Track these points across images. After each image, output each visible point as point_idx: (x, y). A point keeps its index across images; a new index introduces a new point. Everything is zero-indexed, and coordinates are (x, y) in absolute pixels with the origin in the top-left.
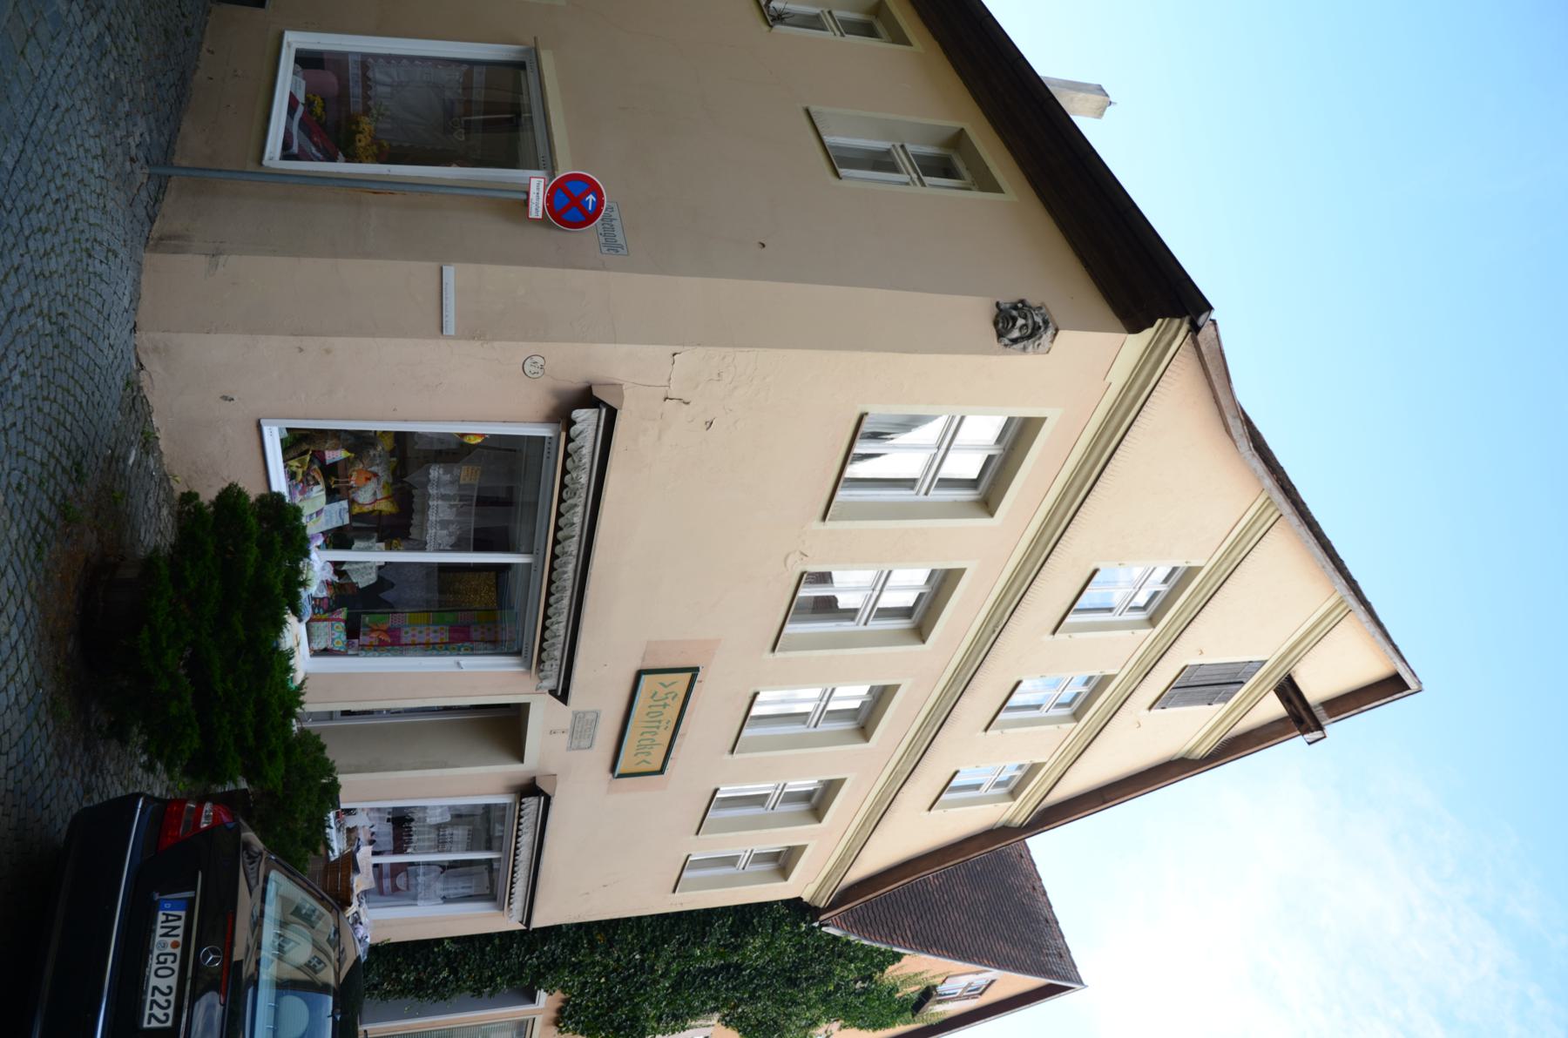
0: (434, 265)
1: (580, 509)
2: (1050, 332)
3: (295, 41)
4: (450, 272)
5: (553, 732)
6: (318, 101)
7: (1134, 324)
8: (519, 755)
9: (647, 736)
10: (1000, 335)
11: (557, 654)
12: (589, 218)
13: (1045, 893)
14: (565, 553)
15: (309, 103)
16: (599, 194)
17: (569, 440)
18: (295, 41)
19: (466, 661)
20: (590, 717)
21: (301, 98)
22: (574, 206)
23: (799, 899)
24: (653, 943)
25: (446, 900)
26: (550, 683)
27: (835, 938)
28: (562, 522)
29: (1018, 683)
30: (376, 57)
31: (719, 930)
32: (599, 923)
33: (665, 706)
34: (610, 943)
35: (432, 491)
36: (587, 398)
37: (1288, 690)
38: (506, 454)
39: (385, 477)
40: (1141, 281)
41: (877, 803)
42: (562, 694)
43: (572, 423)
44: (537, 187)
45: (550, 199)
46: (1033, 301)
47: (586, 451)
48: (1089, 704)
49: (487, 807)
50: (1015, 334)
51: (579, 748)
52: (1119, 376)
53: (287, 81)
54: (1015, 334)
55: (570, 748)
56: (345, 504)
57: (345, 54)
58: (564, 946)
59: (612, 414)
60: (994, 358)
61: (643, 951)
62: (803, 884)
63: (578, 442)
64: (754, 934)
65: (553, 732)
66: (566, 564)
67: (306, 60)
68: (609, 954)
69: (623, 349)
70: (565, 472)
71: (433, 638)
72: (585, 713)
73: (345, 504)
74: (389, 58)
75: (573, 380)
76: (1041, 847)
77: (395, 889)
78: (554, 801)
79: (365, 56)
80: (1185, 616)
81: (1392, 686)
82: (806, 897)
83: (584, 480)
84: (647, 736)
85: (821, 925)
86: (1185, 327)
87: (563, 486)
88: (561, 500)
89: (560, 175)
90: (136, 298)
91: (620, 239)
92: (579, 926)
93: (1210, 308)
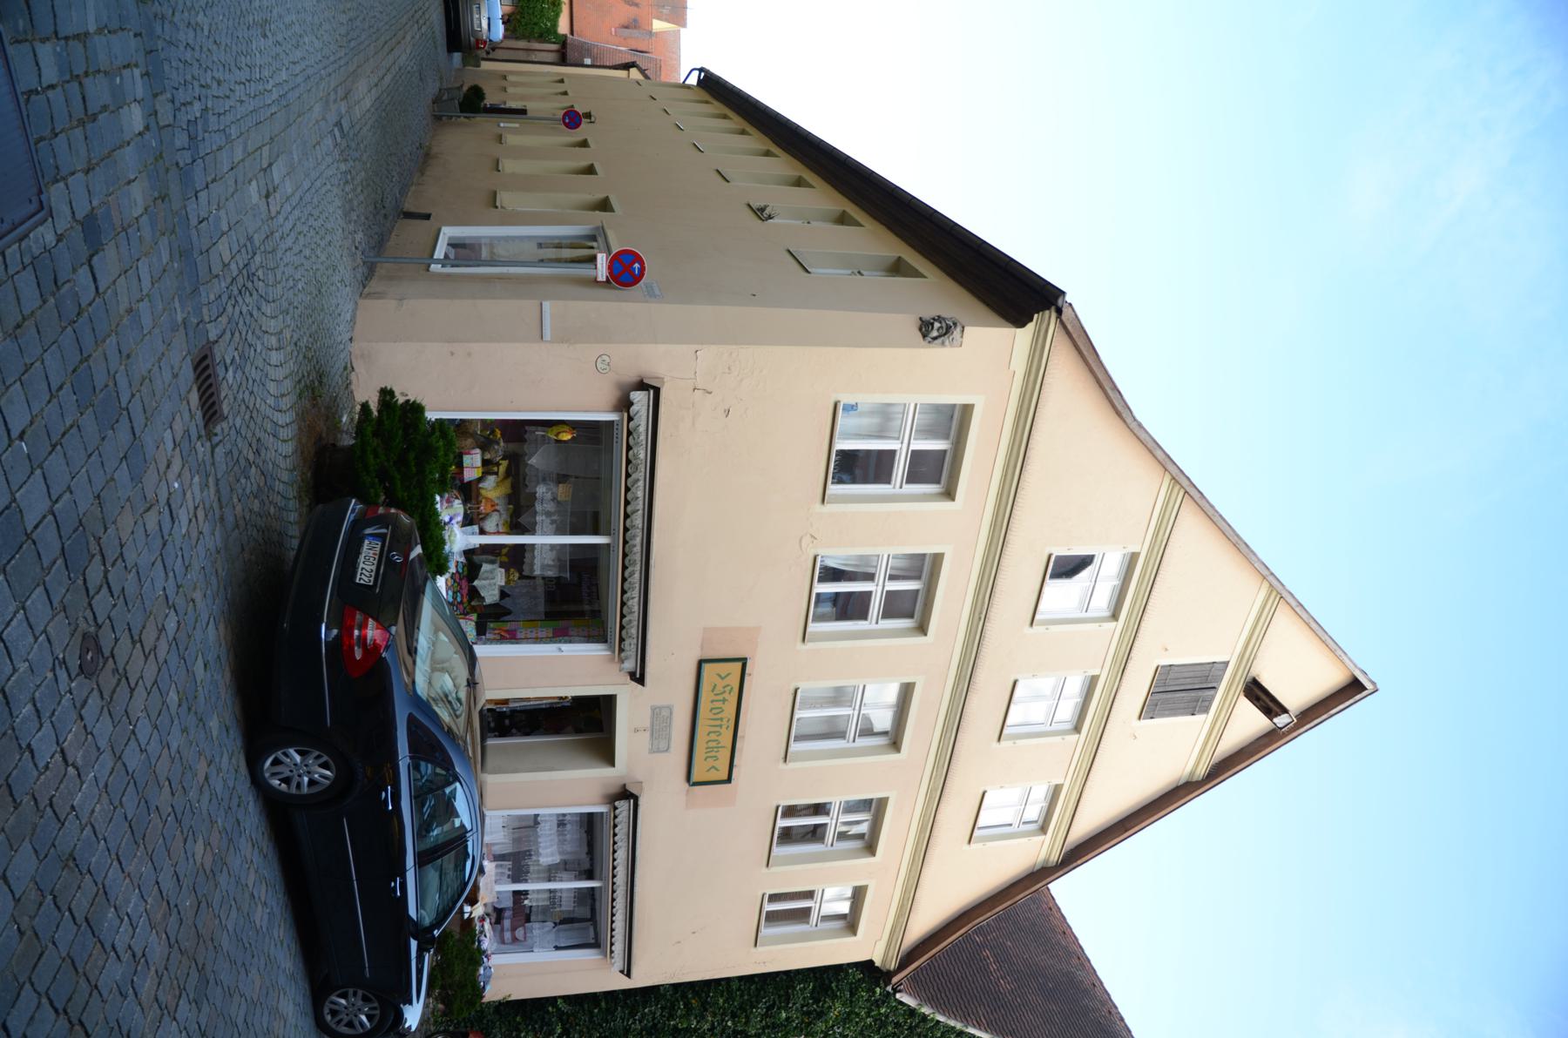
0: (537, 303)
1: (641, 483)
2: (959, 329)
3: (448, 232)
4: (547, 305)
5: (636, 731)
7: (1019, 320)
8: (610, 759)
9: (713, 736)
10: (924, 336)
11: (634, 631)
12: (636, 279)
13: (1122, 1019)
16: (642, 263)
17: (630, 419)
19: (565, 647)
20: (665, 713)
22: (626, 272)
23: (869, 964)
24: (742, 1008)
25: (557, 948)
26: (630, 665)
27: (912, 1012)
28: (630, 496)
29: (1015, 683)
31: (803, 991)
32: (692, 985)
33: (724, 700)
34: (704, 1006)
35: (538, 507)
36: (642, 386)
37: (1257, 693)
38: (592, 433)
39: (505, 516)
40: (1015, 293)
41: (921, 830)
42: (639, 678)
45: (610, 268)
46: (943, 315)
47: (642, 429)
49: (591, 815)
50: (935, 334)
51: (659, 751)
52: (1019, 364)
54: (935, 334)
55: (652, 751)
58: (663, 1008)
59: (657, 391)
60: (922, 351)
61: (734, 1016)
62: (870, 945)
64: (834, 997)
65: (636, 731)
66: (634, 537)
68: (703, 1017)
69: (662, 348)
70: (629, 448)
72: (661, 708)
74: (507, 239)
75: (631, 376)
77: (515, 940)
78: (641, 802)
79: (492, 238)
81: (1353, 688)
83: (642, 456)
84: (713, 736)
85: (895, 991)
86: (1054, 315)
87: (628, 462)
88: (628, 475)
89: (614, 251)
90: (353, 320)
92: (676, 986)
93: (1063, 293)
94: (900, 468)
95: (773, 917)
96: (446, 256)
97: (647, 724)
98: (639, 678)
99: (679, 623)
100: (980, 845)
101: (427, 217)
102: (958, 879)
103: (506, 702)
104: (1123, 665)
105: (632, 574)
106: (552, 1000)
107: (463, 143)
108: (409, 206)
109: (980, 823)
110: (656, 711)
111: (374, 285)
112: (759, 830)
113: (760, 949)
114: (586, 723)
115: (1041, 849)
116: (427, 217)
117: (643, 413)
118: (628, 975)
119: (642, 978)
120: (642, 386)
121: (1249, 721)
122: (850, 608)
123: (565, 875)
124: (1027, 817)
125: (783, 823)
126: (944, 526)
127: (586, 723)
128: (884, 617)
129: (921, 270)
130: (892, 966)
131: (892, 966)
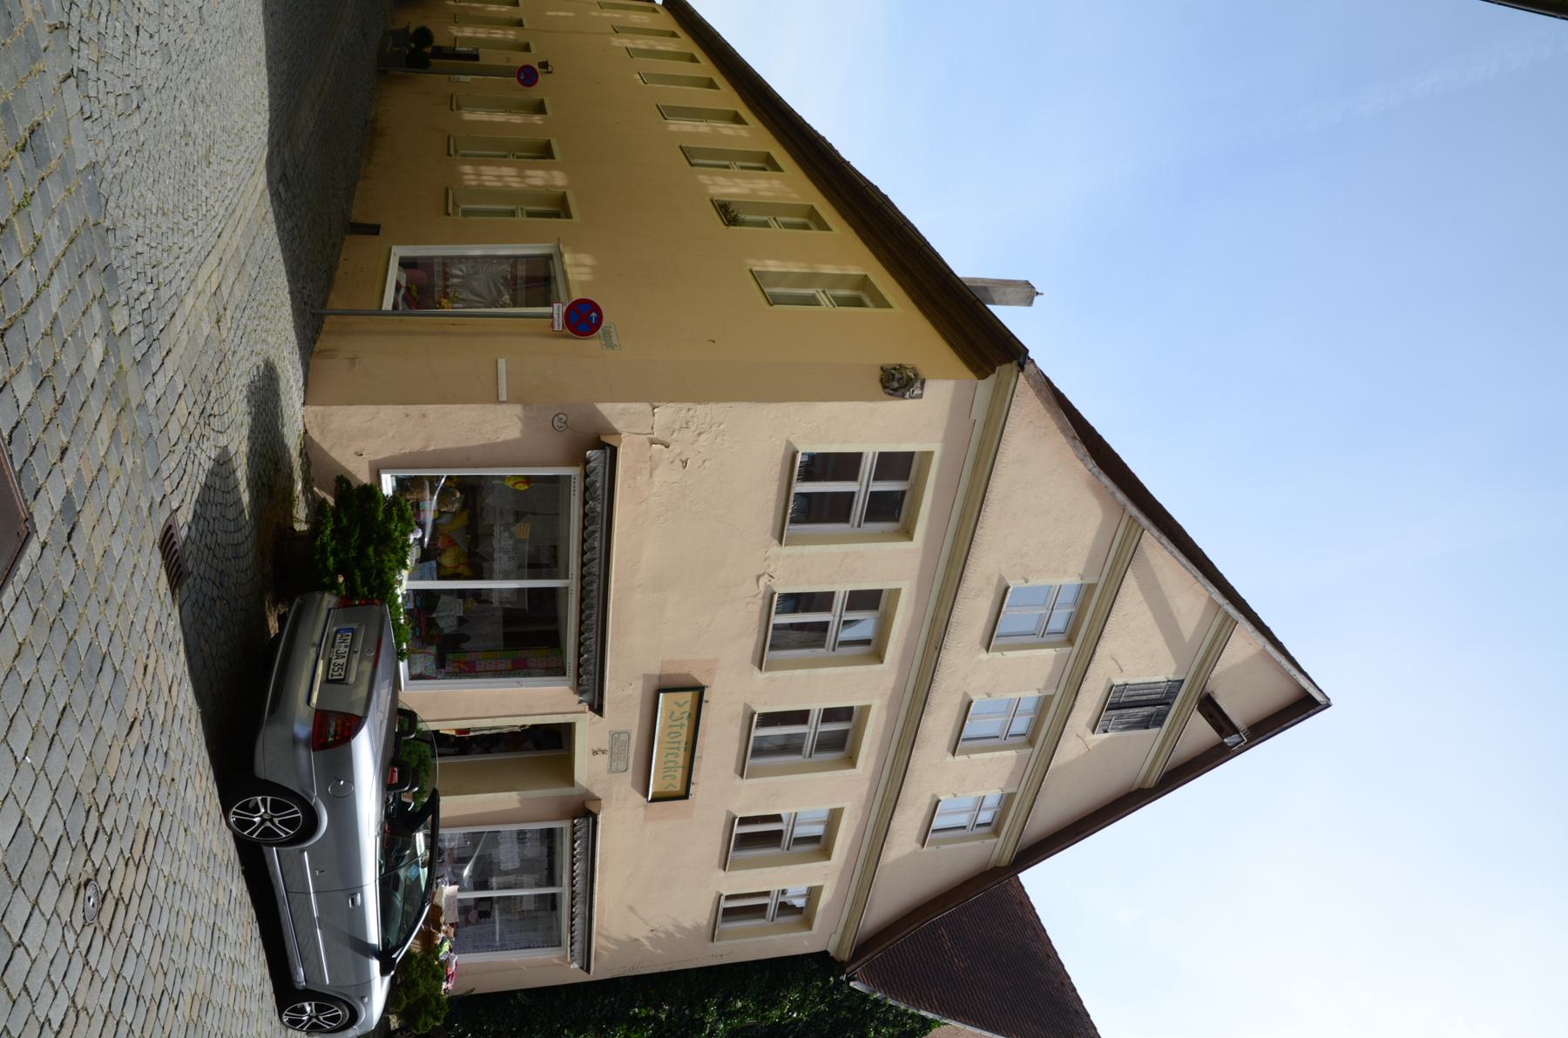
3: (399, 252)
5: (595, 753)
6: (414, 288)
9: (671, 758)
13: (1074, 990)
14: (590, 574)
15: (407, 288)
18: (399, 252)
20: (624, 737)
21: (403, 283)
23: (825, 953)
30: (452, 258)
37: (1209, 707)
42: (598, 709)
43: (587, 462)
44: (558, 310)
48: (1040, 732)
51: (617, 771)
53: (394, 273)
55: (610, 771)
56: (434, 563)
57: (431, 258)
63: (592, 477)
65: (595, 753)
66: (592, 582)
67: (405, 264)
69: (620, 406)
71: (502, 667)
73: (434, 563)
76: (1033, 880)
80: (1095, 633)
82: (831, 950)
84: (671, 758)
91: (615, 340)
94: (859, 507)
95: (730, 913)
96: (395, 306)
97: (606, 747)
98: (598, 709)
99: (636, 645)
100: (998, 655)
101: (374, 230)
102: (912, 868)
103: (467, 731)
104: (1075, 681)
105: (589, 616)
106: (512, 994)
107: (409, 105)
108: (357, 215)
109: (966, 733)
110: (615, 736)
111: (324, 342)
112: (712, 841)
113: (716, 944)
114: (549, 745)
115: (997, 849)
116: (374, 230)
117: (600, 470)
118: (588, 971)
119: (598, 972)
120: (599, 445)
121: (1200, 732)
122: (832, 510)
123: (526, 878)
124: (1013, 730)
125: (737, 830)
126: (868, 687)
127: (549, 745)
128: (867, 520)
129: (889, 298)
130: (845, 955)
131: (845, 955)
